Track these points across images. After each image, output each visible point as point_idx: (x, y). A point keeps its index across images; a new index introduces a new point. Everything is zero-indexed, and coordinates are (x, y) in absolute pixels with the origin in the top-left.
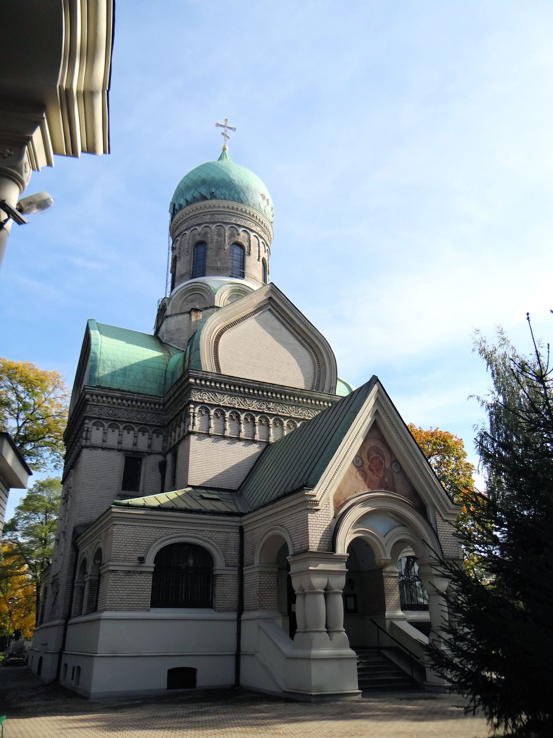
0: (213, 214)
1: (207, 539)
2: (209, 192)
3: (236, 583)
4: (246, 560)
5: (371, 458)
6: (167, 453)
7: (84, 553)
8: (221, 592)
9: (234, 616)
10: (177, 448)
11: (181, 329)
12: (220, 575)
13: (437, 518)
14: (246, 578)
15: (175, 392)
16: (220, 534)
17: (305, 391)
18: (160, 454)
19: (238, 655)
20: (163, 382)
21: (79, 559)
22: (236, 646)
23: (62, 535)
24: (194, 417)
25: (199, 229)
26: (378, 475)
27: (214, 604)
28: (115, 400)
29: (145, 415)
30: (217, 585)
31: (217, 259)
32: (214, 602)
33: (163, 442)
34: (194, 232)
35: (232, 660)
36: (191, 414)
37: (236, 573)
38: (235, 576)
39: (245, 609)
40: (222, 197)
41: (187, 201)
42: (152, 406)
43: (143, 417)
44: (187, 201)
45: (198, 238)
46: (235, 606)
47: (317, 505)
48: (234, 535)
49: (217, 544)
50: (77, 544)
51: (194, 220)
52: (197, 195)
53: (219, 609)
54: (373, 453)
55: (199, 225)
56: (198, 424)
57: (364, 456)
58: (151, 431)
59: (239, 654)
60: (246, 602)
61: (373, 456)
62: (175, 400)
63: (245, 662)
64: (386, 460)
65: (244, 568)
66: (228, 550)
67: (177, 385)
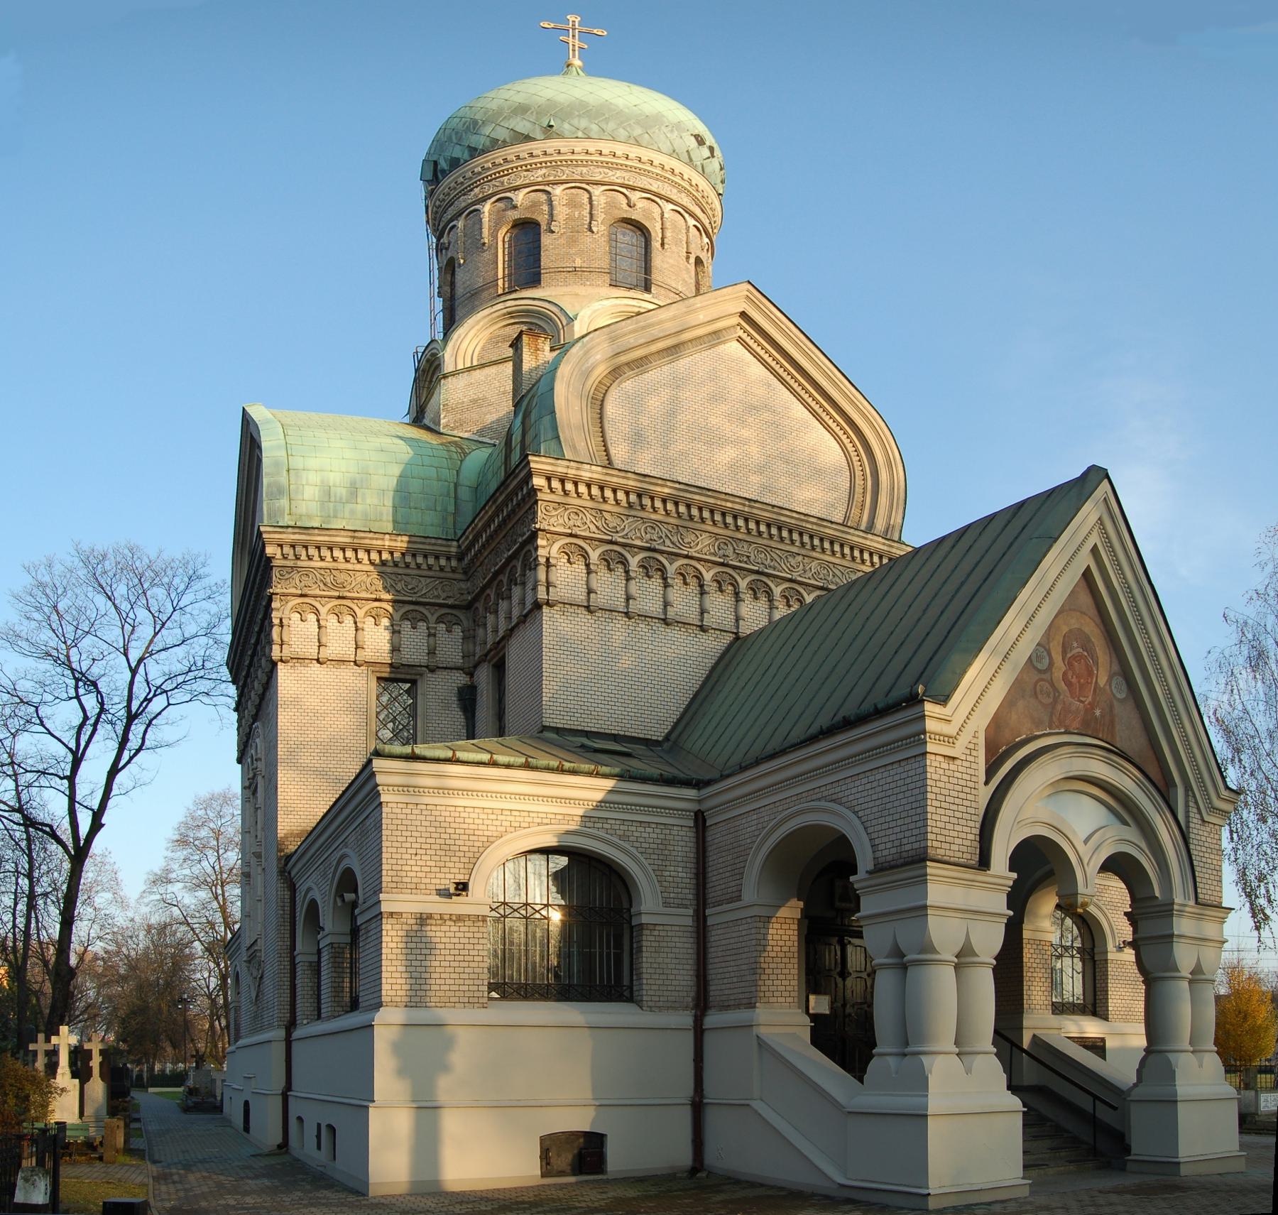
0: (555, 165)
1: (615, 839)
3: (689, 946)
5: (1069, 655)
6: (475, 667)
7: (309, 889)
8: (655, 965)
9: (686, 1019)
10: (504, 647)
11: (484, 399)
12: (651, 927)
13: (1192, 815)
14: (715, 936)
15: (491, 519)
16: (648, 830)
17: (829, 525)
18: (457, 669)
19: (698, 1107)
20: (451, 508)
21: (298, 910)
22: (1036, 1063)
23: (254, 860)
26: (1082, 699)
27: (636, 994)
29: (414, 582)
30: (644, 949)
31: (573, 251)
32: (635, 988)
33: (463, 643)
35: (686, 1115)
36: (540, 559)
37: (689, 921)
38: (686, 929)
39: (711, 1004)
43: (410, 587)
48: (680, 833)
49: (642, 853)
50: (289, 873)
53: (650, 1004)
54: (1075, 645)
58: (432, 619)
59: (701, 1102)
60: (714, 989)
61: (1075, 651)
62: (491, 538)
63: (713, 1119)
64: (1101, 669)
65: (708, 912)
66: (668, 868)
67: (495, 502)
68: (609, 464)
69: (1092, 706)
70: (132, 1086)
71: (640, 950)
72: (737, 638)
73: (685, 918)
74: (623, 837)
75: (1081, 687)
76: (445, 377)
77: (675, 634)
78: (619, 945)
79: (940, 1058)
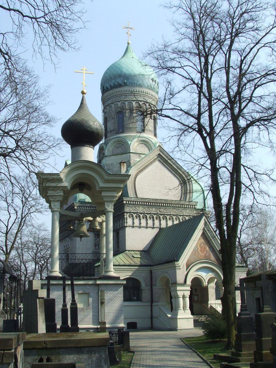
2: (123, 82)
4: (153, 284)
9: (150, 304)
11: (113, 164)
14: (154, 290)
19: (152, 318)
22: (151, 314)
24: (127, 219)
25: (119, 104)
28: (87, 208)
34: (116, 105)
37: (150, 288)
40: (130, 84)
41: (111, 86)
44: (111, 86)
45: (119, 110)
46: (150, 300)
47: (180, 267)
51: (115, 98)
52: (116, 83)
55: (119, 102)
56: (129, 221)
57: (199, 245)
63: (154, 320)
65: (153, 287)
68: (137, 197)
69: (206, 254)
71: (142, 293)
72: (160, 229)
73: (149, 287)
74: (139, 275)
75: (203, 251)
76: (106, 156)
77: (148, 229)
78: (139, 292)
79: (180, 311)
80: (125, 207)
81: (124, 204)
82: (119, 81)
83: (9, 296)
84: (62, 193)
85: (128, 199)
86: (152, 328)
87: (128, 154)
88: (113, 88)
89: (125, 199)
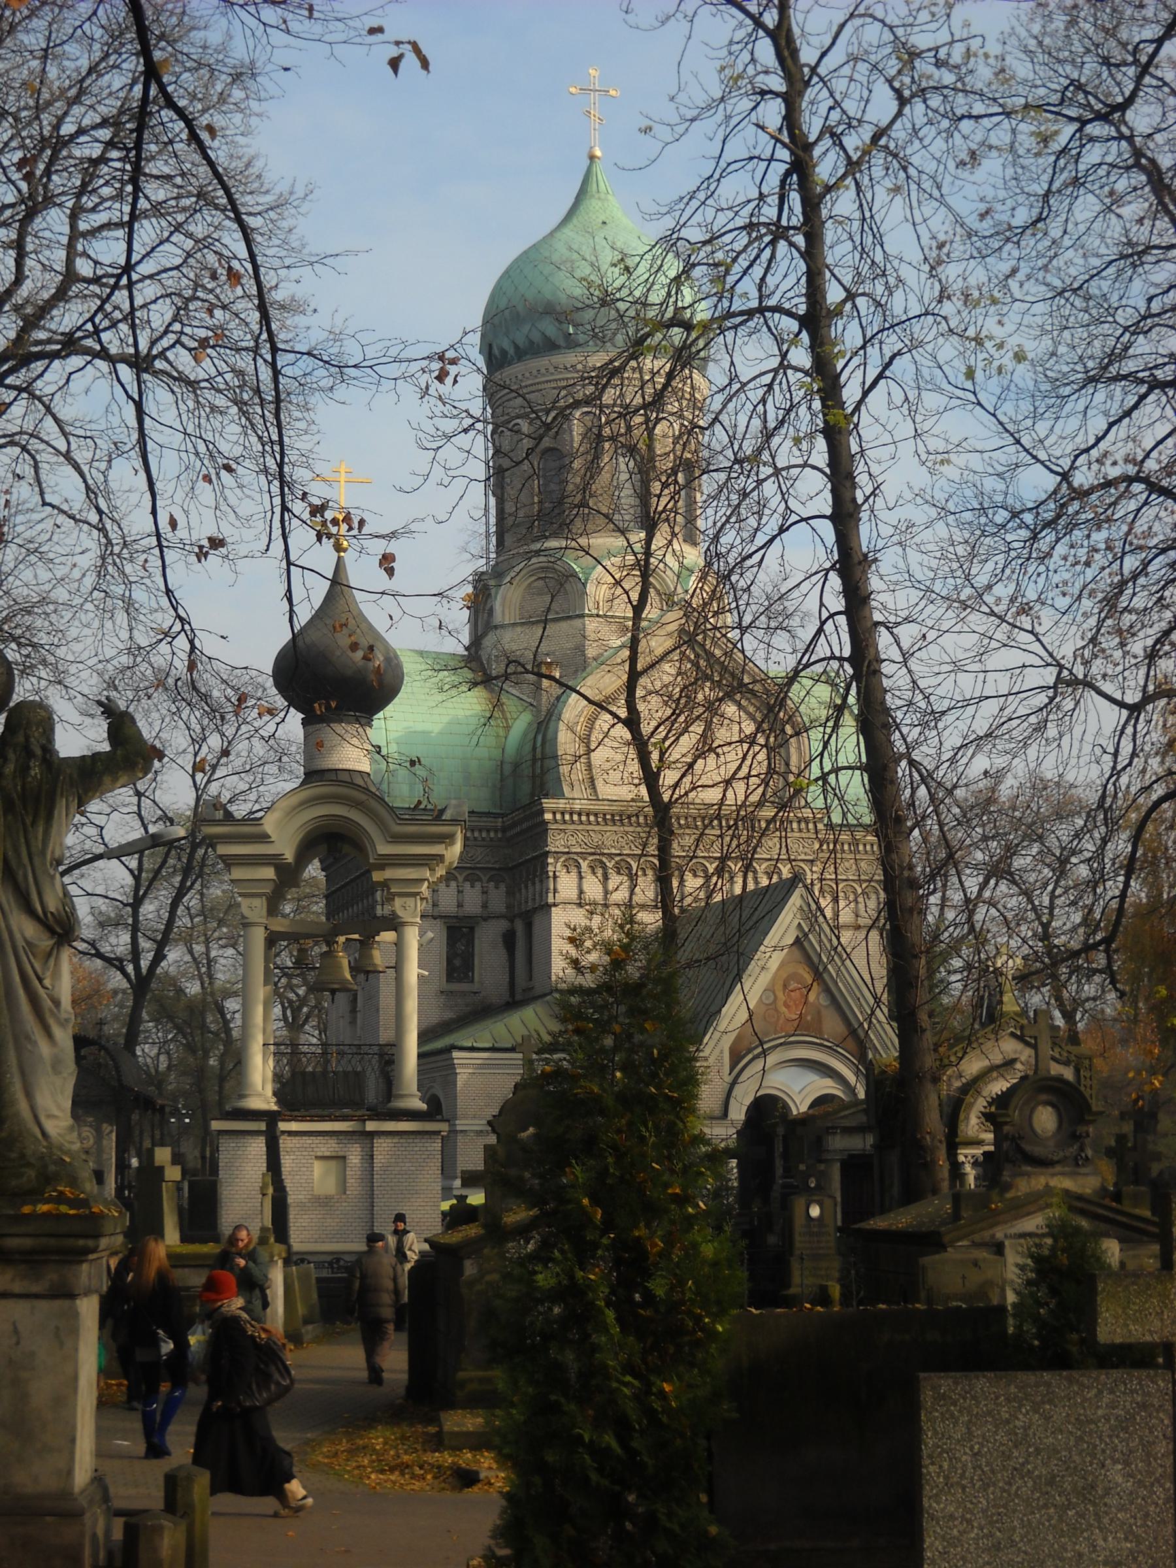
24: (555, 877)
41: (516, 347)
42: (484, 835)
44: (516, 347)
52: (536, 337)
58: (485, 879)
70: (154, 1145)
76: (496, 627)
80: (550, 833)
81: (545, 823)
82: (549, 328)
83: (133, 1152)
84: (269, 873)
85: (561, 804)
86: (1060, 1361)
87: (577, 623)
88: (526, 353)
89: (548, 803)
